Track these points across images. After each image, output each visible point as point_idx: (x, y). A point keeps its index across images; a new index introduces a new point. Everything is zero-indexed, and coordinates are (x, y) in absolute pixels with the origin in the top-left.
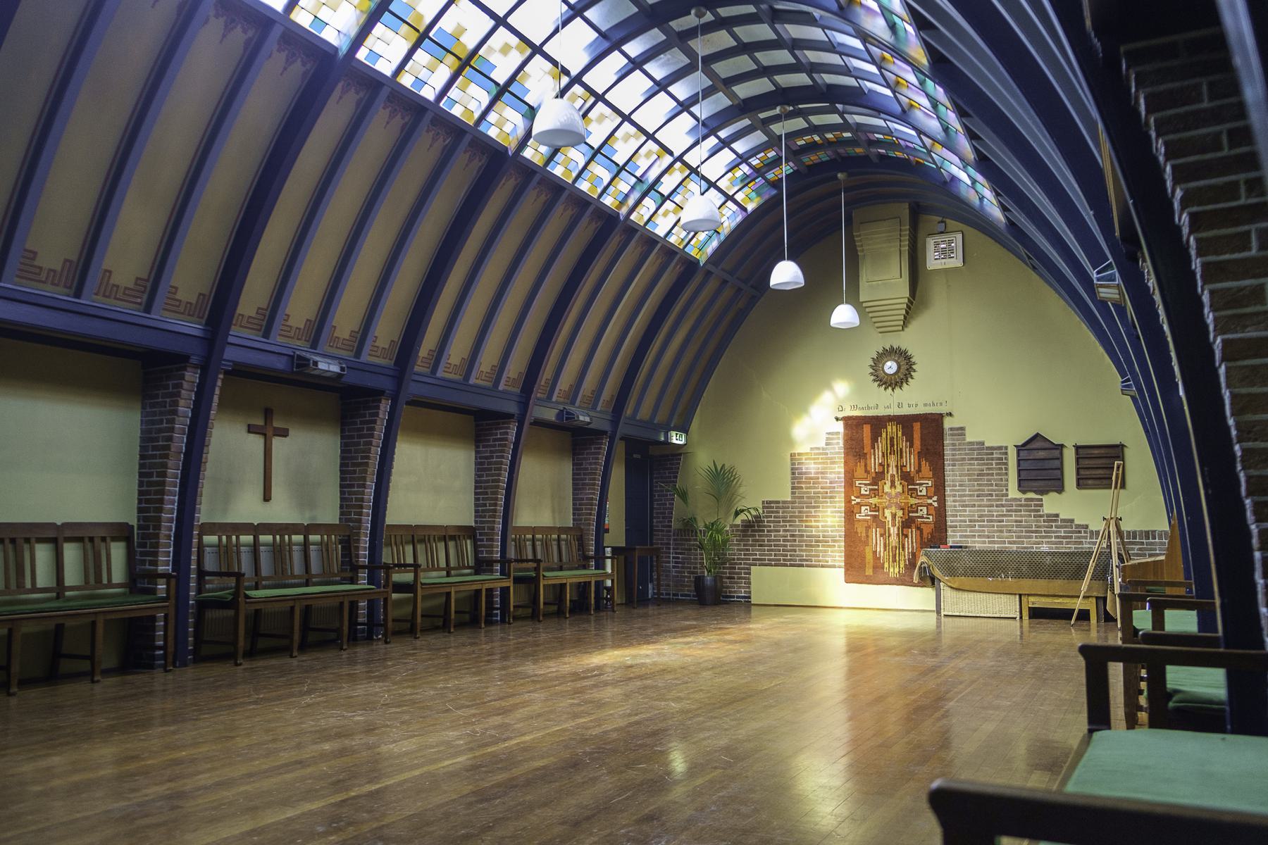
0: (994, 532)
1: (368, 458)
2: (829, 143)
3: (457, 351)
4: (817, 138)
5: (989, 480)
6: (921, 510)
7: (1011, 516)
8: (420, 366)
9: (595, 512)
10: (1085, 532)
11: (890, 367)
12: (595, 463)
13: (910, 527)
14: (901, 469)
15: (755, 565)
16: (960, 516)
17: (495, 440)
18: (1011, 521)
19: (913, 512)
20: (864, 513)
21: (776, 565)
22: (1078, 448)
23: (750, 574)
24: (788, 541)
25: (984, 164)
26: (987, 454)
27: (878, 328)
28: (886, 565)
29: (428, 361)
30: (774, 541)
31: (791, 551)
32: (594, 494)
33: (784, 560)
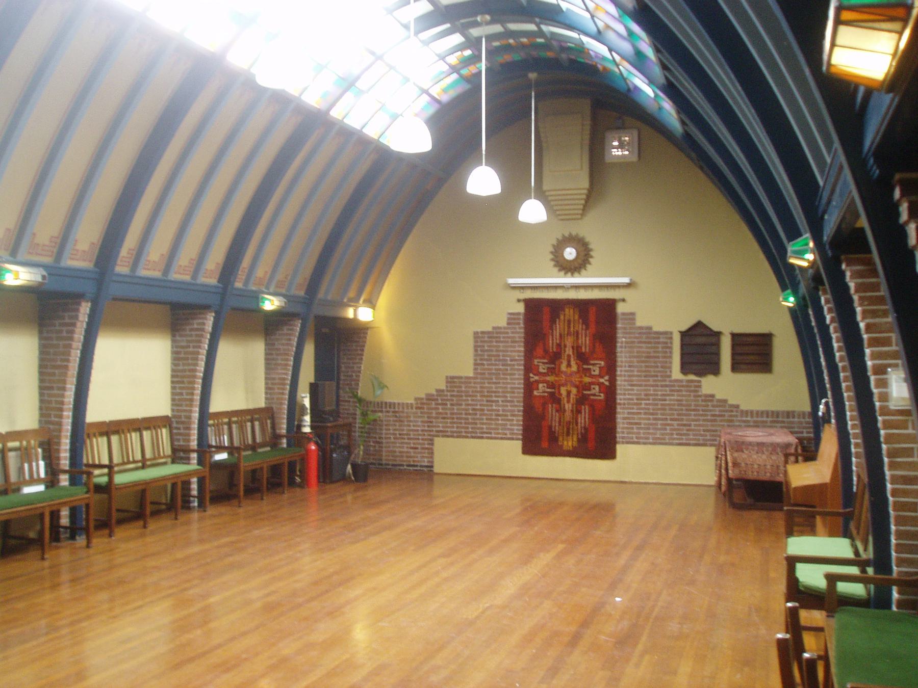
0: (659, 409)
1: (68, 361)
2: (523, 46)
3: (157, 251)
4: (511, 41)
5: (655, 362)
6: (594, 388)
7: (673, 395)
8: (122, 268)
9: (287, 392)
10: (737, 412)
11: (570, 253)
12: (287, 344)
13: (583, 404)
14: (577, 350)
15: (438, 436)
16: (629, 394)
17: (191, 330)
18: (674, 400)
19: (586, 390)
20: (541, 390)
21: (458, 437)
22: (734, 336)
23: (432, 444)
24: (470, 414)
25: (671, 90)
26: (654, 338)
27: (559, 215)
28: (561, 439)
29: (128, 260)
30: (456, 414)
31: (472, 423)
32: (286, 374)
33: (466, 432)
